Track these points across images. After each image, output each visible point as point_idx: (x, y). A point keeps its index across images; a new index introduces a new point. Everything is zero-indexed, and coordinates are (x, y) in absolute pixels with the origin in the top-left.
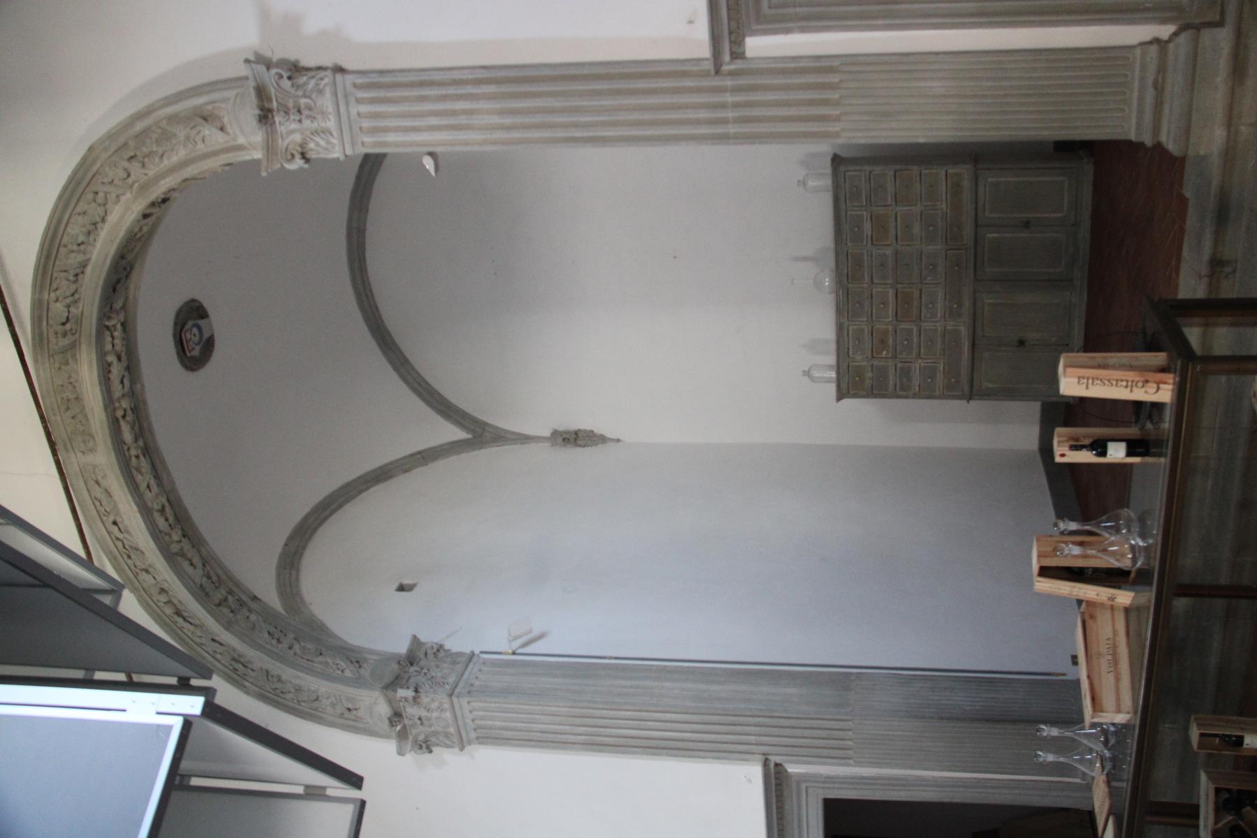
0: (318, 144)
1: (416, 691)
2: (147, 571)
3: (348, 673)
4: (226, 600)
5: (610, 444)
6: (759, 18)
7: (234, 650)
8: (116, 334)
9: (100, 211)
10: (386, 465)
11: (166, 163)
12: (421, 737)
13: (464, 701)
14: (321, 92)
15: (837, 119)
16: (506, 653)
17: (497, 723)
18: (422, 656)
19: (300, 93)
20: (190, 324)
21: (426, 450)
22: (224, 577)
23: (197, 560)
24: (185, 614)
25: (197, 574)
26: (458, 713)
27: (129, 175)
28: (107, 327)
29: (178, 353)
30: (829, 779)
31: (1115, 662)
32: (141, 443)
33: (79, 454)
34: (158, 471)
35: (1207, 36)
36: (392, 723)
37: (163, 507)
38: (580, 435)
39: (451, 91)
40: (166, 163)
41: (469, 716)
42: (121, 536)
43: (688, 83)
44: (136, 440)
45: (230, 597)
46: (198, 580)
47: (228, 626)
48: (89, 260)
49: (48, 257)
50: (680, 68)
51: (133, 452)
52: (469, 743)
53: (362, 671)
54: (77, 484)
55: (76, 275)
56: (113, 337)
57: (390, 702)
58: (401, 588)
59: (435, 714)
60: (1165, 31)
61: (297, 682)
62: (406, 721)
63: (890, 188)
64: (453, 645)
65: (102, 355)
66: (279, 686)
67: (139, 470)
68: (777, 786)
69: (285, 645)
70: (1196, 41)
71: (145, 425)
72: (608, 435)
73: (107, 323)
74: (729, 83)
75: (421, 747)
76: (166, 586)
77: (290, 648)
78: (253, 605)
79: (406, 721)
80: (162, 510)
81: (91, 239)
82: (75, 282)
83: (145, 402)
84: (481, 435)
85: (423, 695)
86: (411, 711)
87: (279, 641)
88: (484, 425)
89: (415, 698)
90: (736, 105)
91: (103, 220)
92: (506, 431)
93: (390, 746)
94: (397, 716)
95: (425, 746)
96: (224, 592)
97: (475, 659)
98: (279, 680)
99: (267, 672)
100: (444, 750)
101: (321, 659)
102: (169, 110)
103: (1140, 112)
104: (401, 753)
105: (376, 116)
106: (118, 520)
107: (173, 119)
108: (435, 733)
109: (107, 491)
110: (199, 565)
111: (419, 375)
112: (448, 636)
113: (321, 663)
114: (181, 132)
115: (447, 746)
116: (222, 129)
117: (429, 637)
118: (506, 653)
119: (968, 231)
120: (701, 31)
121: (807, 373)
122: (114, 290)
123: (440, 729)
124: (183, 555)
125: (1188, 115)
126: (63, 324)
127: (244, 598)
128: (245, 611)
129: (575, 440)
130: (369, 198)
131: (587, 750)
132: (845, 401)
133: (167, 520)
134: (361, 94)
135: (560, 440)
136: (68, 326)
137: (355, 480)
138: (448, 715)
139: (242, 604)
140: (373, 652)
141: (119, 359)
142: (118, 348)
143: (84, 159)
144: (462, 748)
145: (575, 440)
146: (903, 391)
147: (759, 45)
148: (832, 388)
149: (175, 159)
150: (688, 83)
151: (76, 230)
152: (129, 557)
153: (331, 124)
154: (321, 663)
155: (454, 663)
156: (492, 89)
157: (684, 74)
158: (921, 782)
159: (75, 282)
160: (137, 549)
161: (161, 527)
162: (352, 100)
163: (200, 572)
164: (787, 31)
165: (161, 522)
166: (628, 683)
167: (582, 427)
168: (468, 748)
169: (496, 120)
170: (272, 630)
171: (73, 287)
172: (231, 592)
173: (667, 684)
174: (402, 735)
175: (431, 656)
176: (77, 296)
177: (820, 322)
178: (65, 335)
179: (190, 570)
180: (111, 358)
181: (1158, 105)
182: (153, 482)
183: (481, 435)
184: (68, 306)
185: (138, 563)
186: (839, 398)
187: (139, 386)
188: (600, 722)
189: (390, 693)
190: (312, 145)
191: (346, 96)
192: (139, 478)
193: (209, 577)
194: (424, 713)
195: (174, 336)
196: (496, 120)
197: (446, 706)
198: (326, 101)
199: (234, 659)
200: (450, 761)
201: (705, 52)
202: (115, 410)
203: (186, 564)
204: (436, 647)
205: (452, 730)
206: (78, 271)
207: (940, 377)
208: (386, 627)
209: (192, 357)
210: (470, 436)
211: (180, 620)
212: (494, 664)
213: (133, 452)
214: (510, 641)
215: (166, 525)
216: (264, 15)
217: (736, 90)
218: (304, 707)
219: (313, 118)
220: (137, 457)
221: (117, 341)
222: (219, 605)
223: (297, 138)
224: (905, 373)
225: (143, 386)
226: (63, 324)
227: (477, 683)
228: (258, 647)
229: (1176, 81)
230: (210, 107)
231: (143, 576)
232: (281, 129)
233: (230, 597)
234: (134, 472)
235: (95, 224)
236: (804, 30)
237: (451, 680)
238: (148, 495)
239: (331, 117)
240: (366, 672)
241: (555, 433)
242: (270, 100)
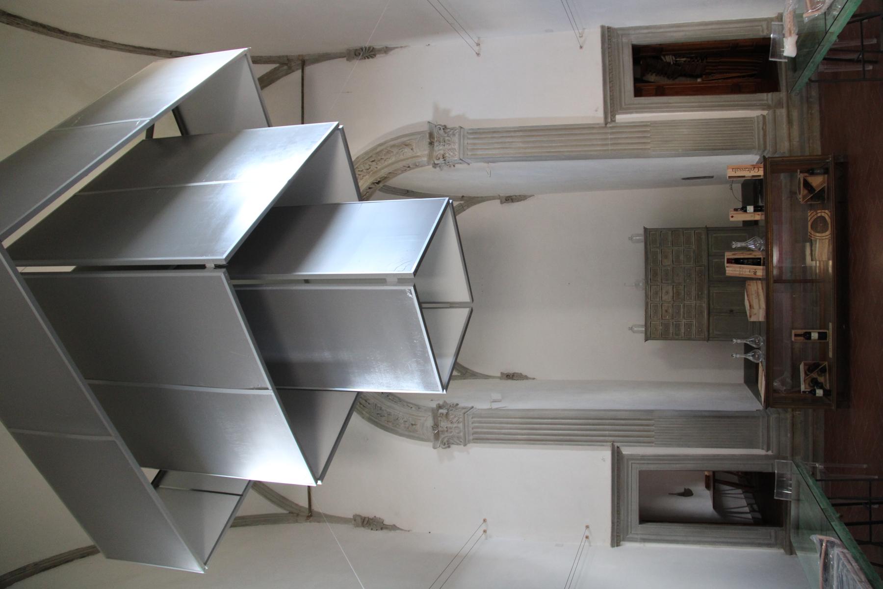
6: (621, 108)
11: (386, 163)
12: (445, 440)
14: (454, 135)
15: (649, 143)
30: (643, 458)
31: (758, 295)
35: (778, 111)
39: (505, 135)
40: (386, 163)
43: (595, 131)
52: (469, 442)
59: (455, 425)
60: (765, 113)
63: (670, 238)
68: (618, 461)
70: (775, 112)
74: (610, 131)
79: (440, 429)
86: (444, 424)
88: (466, 369)
90: (611, 139)
95: (447, 445)
98: (381, 409)
102: (392, 143)
103: (759, 139)
105: (475, 144)
107: (393, 146)
114: (395, 150)
115: (458, 444)
119: (705, 261)
120: (600, 114)
121: (631, 329)
125: (775, 138)
132: (649, 341)
138: (461, 425)
144: (465, 445)
146: (676, 337)
147: (621, 118)
148: (643, 336)
149: (390, 161)
150: (595, 131)
153: (456, 147)
156: (521, 134)
157: (593, 128)
158: (686, 458)
164: (631, 113)
167: (517, 371)
168: (468, 445)
169: (521, 145)
177: (638, 317)
181: (765, 135)
186: (646, 340)
194: (450, 425)
196: (521, 145)
198: (456, 139)
200: (457, 452)
201: (602, 121)
207: (694, 328)
216: (436, 109)
217: (612, 133)
218: (390, 425)
223: (442, 152)
224: (677, 326)
229: (770, 127)
232: (436, 148)
236: (637, 112)
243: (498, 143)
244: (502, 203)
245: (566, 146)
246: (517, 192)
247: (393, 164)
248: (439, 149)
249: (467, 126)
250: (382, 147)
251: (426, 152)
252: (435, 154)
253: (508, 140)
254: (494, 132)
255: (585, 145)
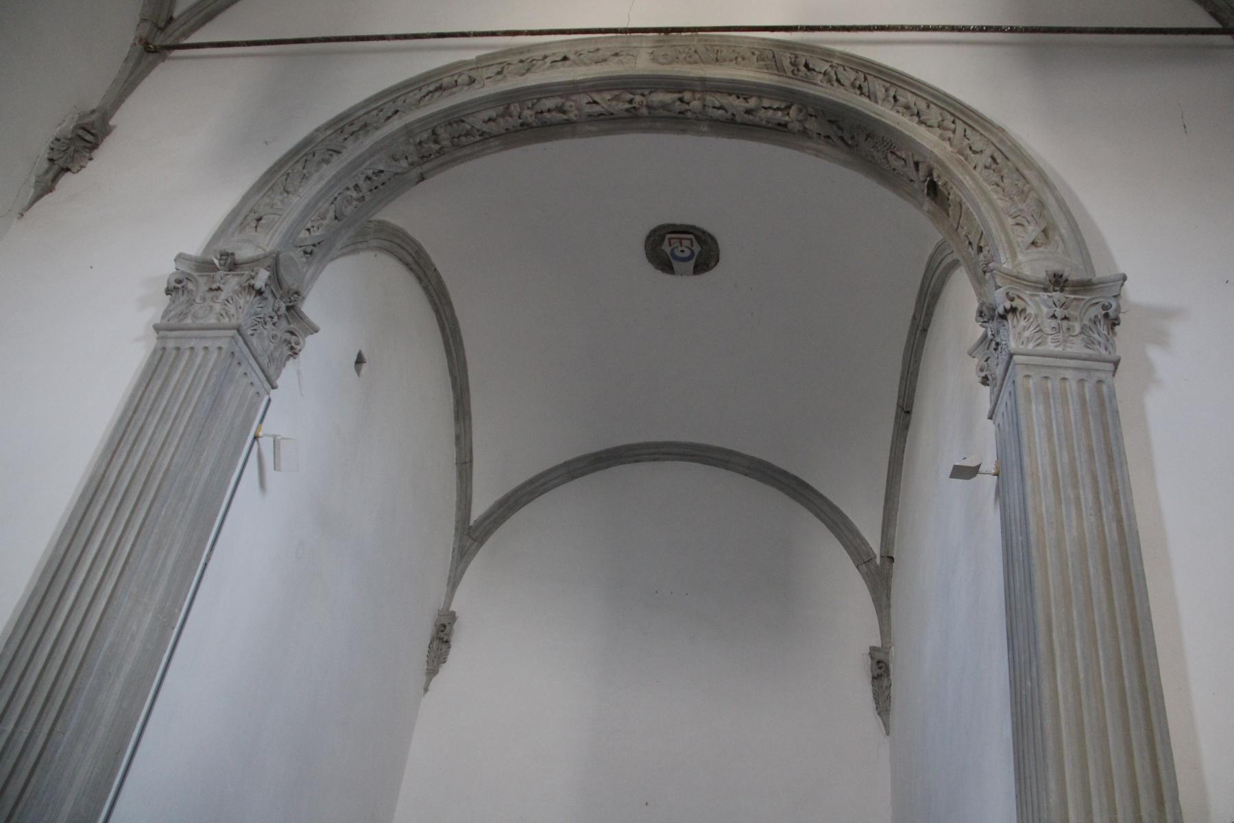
0: (1025, 329)
1: (260, 293)
2: (499, 73)
3: (304, 234)
4: (436, 142)
5: (423, 679)
7: (377, 128)
8: (780, 113)
9: (934, 121)
10: (470, 419)
12: (190, 286)
13: (224, 344)
16: (259, 428)
17: (176, 376)
18: (293, 326)
19: (1086, 322)
20: (697, 249)
21: (471, 467)
22: (459, 153)
23: (492, 128)
24: (437, 94)
25: (477, 121)
26: (208, 333)
27: (975, 152)
28: (789, 107)
29: (674, 225)
32: (644, 111)
33: (650, 51)
34: (607, 122)
36: (225, 255)
37: (564, 112)
38: (444, 647)
41: (199, 345)
42: (548, 60)
44: (648, 107)
45: (437, 147)
46: (470, 119)
47: (408, 130)
48: (876, 102)
49: (880, 72)
50: (1167, 798)
51: (638, 98)
53: (299, 251)
54: (616, 41)
55: (860, 88)
56: (778, 109)
57: (255, 261)
58: (360, 360)
59: (218, 307)
61: (315, 176)
62: (221, 273)
64: (288, 375)
65: (759, 90)
66: (317, 158)
67: (616, 98)
69: (361, 183)
71: (658, 125)
72: (435, 680)
73: (794, 108)
75: (179, 282)
76: (476, 85)
77: (356, 187)
78: (415, 172)
80: (560, 109)
81: (900, 109)
82: (853, 85)
83: (684, 131)
84: (472, 535)
85: (251, 298)
86: (232, 283)
87: (368, 178)
88: (481, 541)
89: (252, 287)
91: (921, 122)
92: (467, 563)
93: (195, 247)
94: (233, 265)
96: (446, 143)
97: (267, 386)
99: (338, 152)
100: (162, 309)
101: (331, 214)
104: (180, 258)
106: (567, 63)
107: (1041, 204)
108: (191, 303)
109: (605, 60)
110: (485, 128)
111: (554, 487)
112: (299, 373)
113: (327, 211)
115: (166, 312)
116: (1033, 243)
117: (310, 344)
118: (259, 428)
122: (831, 122)
123: (195, 308)
124: (506, 113)
126: (806, 66)
127: (427, 166)
128: (415, 158)
129: (441, 639)
130: (760, 480)
131: (91, 480)
133: (549, 111)
134: (1088, 386)
135: (444, 621)
136: (803, 69)
137: (467, 376)
138: (212, 320)
139: (425, 158)
140: (314, 278)
141: (748, 112)
142: (762, 113)
143: (990, 122)
144: (157, 328)
145: (441, 639)
151: (907, 98)
152: (522, 61)
153: (1050, 347)
154: (327, 211)
155: (271, 359)
156: (1112, 534)
159: (853, 85)
160: (528, 70)
161: (544, 101)
162: (1084, 375)
163: (479, 125)
165: (549, 103)
166: (170, 563)
167: (452, 652)
168: (154, 335)
170: (383, 177)
171: (847, 83)
172: (441, 152)
173: (149, 618)
174: (204, 266)
175: (288, 336)
176: (836, 84)
178: (794, 64)
179: (485, 115)
180: (753, 103)
182: (596, 109)
183: (472, 535)
184: (825, 74)
185: (511, 67)
187: (705, 129)
188: (129, 506)
189: (269, 262)
190: (1023, 323)
191: (1088, 370)
192: (607, 96)
193: (467, 134)
194: (223, 296)
195: (694, 227)
197: (226, 321)
199: (366, 125)
202: (694, 91)
203: (492, 113)
204: (298, 347)
205: (189, 321)
206: (865, 90)
208: (344, 299)
209: (663, 239)
210: (472, 523)
211: (432, 88)
212: (253, 406)
213: (638, 98)
214: (275, 437)
215: (545, 108)
219: (1058, 329)
220: (631, 101)
221: (770, 112)
222: (434, 133)
223: (1031, 310)
225: (702, 134)
226: (806, 66)
227: (241, 370)
228: (372, 152)
230: (1057, 238)
231: (496, 69)
233: (437, 147)
234: (616, 93)
235: (918, 114)
237: (254, 341)
238: (584, 99)
239: (1060, 349)
240: (297, 255)
241: (453, 617)
242: (1074, 292)
243: (1072, 460)
244: (873, 650)
245: (1077, 688)
246: (896, 692)
247: (991, 202)
248: (1038, 305)
249: (1122, 383)
250: (1035, 182)
251: (1027, 271)
252: (1026, 294)
253: (1087, 496)
254: (1110, 456)
255: (1084, 768)
